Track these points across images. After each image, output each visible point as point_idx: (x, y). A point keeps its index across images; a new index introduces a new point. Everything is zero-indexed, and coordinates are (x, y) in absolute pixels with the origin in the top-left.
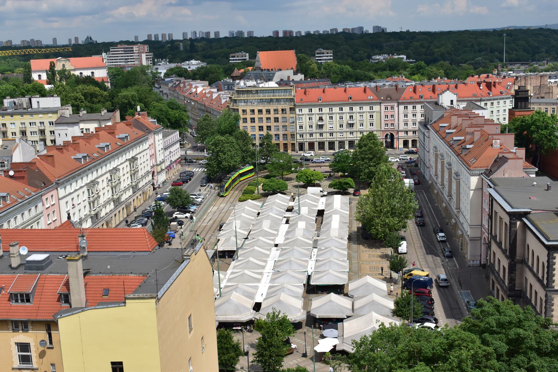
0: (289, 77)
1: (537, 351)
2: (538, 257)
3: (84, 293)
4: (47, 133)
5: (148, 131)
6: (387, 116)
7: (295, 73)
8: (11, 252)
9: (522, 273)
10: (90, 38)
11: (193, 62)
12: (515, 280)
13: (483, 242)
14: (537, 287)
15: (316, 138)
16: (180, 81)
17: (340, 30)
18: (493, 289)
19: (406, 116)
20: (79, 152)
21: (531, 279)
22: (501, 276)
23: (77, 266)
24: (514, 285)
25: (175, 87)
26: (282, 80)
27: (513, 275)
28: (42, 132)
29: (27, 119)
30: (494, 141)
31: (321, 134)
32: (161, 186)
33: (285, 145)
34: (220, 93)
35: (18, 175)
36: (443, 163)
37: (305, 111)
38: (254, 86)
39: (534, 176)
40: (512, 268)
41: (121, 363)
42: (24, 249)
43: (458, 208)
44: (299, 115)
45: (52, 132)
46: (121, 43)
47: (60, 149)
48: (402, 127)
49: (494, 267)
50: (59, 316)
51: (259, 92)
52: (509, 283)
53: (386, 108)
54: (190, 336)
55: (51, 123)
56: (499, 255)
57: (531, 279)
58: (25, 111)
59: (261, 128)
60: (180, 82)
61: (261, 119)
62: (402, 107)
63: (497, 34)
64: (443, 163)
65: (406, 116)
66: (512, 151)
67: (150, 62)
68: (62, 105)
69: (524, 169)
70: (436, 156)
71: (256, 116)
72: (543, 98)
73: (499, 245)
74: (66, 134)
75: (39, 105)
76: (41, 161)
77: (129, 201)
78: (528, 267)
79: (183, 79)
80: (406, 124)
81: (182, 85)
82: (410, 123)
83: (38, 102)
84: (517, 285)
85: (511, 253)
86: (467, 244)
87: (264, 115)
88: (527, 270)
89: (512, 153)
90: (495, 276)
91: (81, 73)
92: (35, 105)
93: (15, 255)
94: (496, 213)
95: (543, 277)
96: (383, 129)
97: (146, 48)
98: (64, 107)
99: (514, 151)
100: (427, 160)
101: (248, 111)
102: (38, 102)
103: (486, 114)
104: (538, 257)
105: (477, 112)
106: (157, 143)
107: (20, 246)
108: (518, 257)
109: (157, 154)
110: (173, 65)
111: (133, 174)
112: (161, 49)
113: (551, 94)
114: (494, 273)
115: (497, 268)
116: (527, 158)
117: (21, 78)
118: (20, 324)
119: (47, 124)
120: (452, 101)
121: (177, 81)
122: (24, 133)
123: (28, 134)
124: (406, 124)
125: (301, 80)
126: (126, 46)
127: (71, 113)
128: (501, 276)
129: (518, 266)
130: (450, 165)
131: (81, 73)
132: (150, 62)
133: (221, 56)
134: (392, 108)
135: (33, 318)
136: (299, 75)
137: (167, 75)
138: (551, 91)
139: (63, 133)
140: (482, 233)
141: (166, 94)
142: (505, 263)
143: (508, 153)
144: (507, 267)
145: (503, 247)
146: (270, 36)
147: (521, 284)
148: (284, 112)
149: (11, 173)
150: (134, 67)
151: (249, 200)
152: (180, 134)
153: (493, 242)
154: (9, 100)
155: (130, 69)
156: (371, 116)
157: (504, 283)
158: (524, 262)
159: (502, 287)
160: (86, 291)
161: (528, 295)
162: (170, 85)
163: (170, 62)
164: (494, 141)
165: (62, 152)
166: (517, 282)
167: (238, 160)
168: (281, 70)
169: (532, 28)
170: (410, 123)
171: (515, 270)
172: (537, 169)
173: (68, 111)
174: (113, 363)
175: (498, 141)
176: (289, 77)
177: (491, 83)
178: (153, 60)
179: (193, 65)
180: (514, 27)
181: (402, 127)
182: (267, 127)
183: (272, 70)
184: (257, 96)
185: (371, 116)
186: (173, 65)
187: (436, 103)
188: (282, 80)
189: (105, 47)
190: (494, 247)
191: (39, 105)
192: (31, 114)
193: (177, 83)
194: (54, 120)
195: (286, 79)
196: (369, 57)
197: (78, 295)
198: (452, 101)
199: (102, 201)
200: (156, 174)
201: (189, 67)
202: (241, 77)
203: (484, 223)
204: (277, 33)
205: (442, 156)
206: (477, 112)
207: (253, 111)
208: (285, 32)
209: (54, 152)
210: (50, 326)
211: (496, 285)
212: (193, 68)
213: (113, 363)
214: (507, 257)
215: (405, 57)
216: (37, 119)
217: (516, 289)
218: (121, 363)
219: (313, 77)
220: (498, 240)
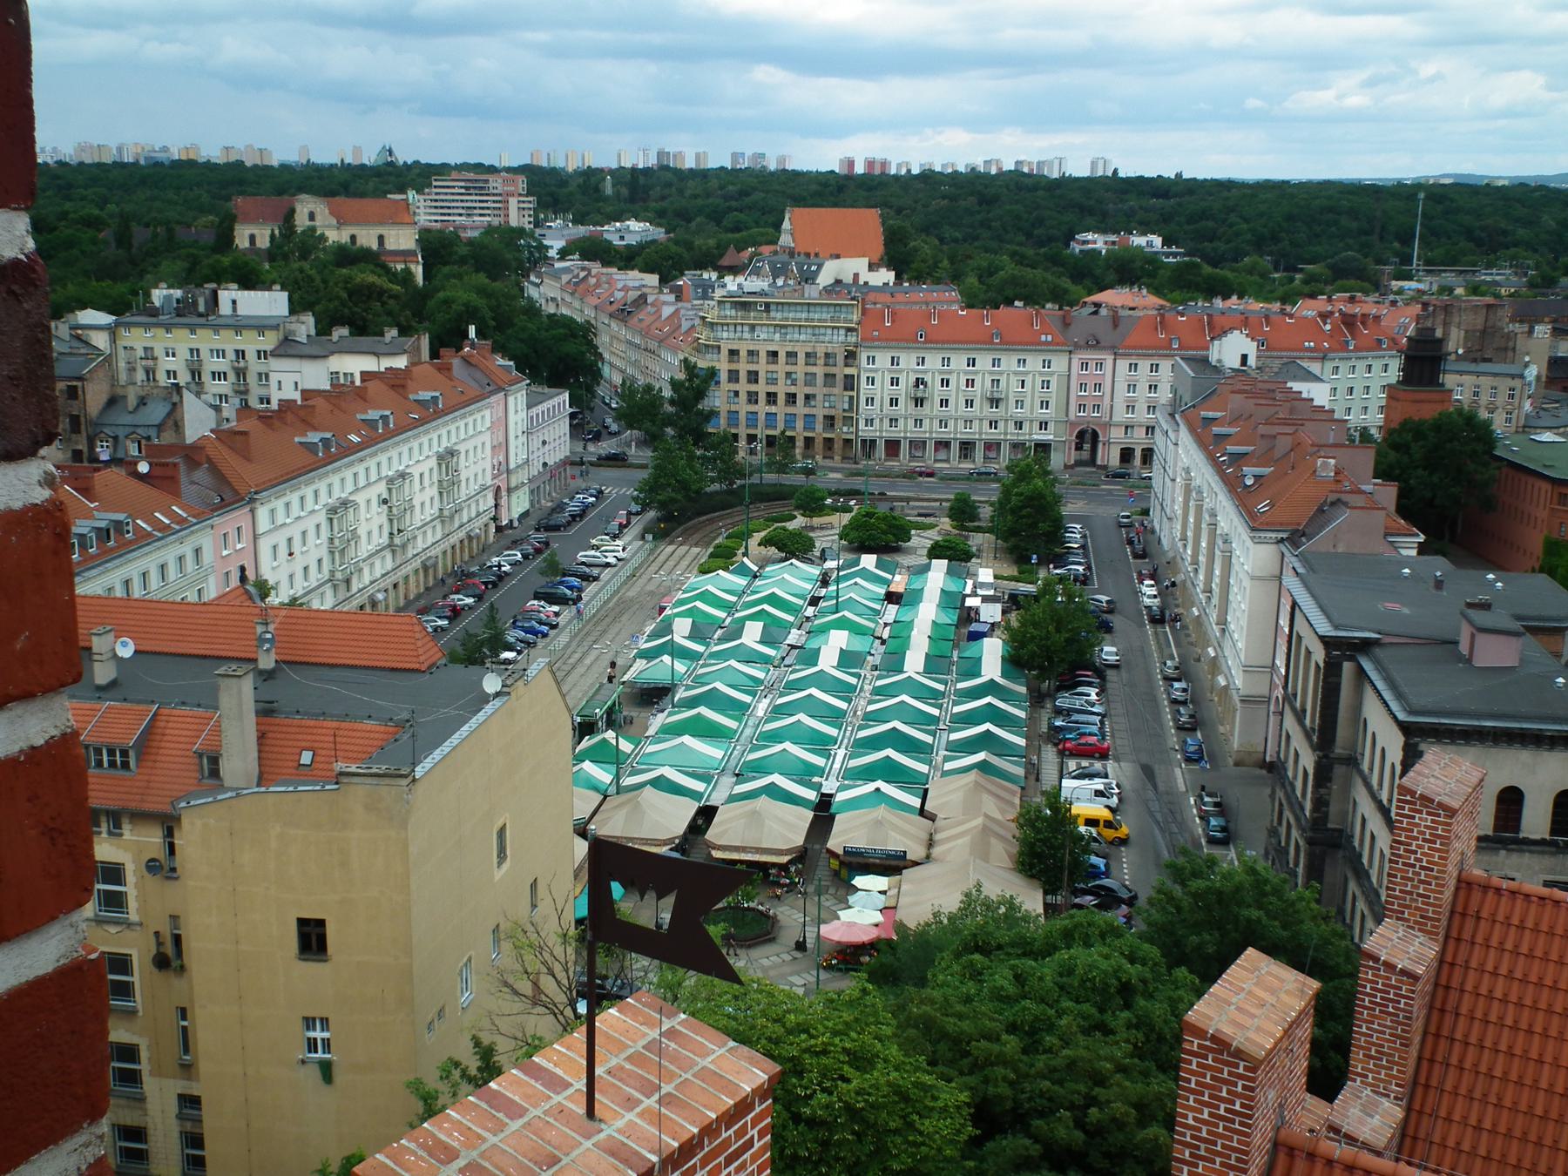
0: (856, 276)
1: (599, 1004)
2: (1383, 750)
3: (256, 755)
4: (252, 379)
5: (498, 387)
6: (1083, 386)
7: (872, 267)
8: (95, 650)
9: (1347, 788)
10: (390, 152)
11: (634, 225)
12: (1327, 804)
13: (1272, 708)
14: (1376, 824)
15: (905, 430)
16: (589, 271)
17: (1008, 165)
18: (1280, 823)
19: (1132, 387)
20: (315, 429)
21: (1366, 807)
22: (1299, 793)
23: (240, 692)
24: (1326, 816)
25: (576, 284)
26: (838, 282)
27: (1322, 791)
28: (241, 373)
29: (205, 340)
30: (1320, 461)
31: (918, 422)
32: (516, 524)
33: (809, 442)
34: (680, 305)
35: (158, 472)
36: (1199, 508)
37: (883, 359)
38: (762, 294)
39: (1414, 553)
40: (1323, 774)
41: (321, 923)
42: (124, 645)
43: (1223, 622)
44: (866, 370)
45: (264, 377)
46: (465, 167)
47: (266, 418)
48: (1121, 415)
49: (1285, 770)
50: (183, 804)
51: (773, 307)
52: (1314, 810)
53: (1084, 365)
54: (498, 874)
55: (260, 354)
56: (1299, 742)
57: (1366, 807)
58: (202, 321)
59: (771, 398)
60: (589, 274)
61: (753, 377)
62: (1123, 365)
63: (1403, 193)
64: (1199, 508)
65: (1132, 387)
66: (1364, 487)
67: (527, 219)
68: (292, 311)
69: (1386, 535)
70: (1188, 490)
71: (762, 366)
72: (1489, 360)
73: (1300, 716)
74: (291, 380)
75: (234, 309)
76: (217, 444)
77: (433, 553)
78: (1361, 772)
79: (596, 267)
80: (1131, 408)
81: (593, 281)
82: (1141, 407)
83: (234, 302)
84: (1332, 817)
85: (1324, 737)
86: (1235, 710)
87: (781, 367)
88: (1359, 782)
89: (1364, 492)
90: (1286, 793)
91: (353, 238)
92: (225, 308)
93: (104, 658)
94: (1299, 638)
95: (1390, 801)
96: (1072, 417)
97: (521, 183)
98: (294, 318)
99: (1368, 488)
100: (1168, 502)
101: (743, 354)
102: (234, 302)
103: (1319, 394)
104: (1383, 750)
105: (1296, 386)
106: (512, 418)
107: (117, 637)
108: (1339, 750)
109: (496, 444)
110: (582, 230)
111: (447, 487)
112: (553, 190)
113: (1510, 354)
114: (1283, 786)
115: (1290, 774)
116: (1404, 510)
117: (208, 238)
118: (103, 819)
119: (251, 356)
120: (1244, 358)
121: (583, 269)
122: (196, 373)
123: (206, 377)
124: (1131, 408)
125: (886, 284)
126: (471, 176)
127: (313, 332)
128: (1299, 793)
129: (1339, 770)
130: (1213, 515)
131: (353, 238)
132: (527, 219)
133: (714, 217)
134: (1100, 365)
135: (133, 805)
136: (883, 271)
137: (564, 254)
138: (1511, 344)
139: (288, 380)
140: (1272, 685)
141: (553, 299)
142: (1308, 760)
143: (1352, 492)
144: (1311, 771)
145: (1308, 722)
146: (832, 172)
147: (1344, 815)
148: (831, 361)
149: (143, 468)
150: (490, 230)
151: (720, 572)
152: (1365, 434)
153: (1287, 707)
154: (165, 292)
155: (476, 234)
156: (1046, 384)
157: (1302, 808)
158: (1352, 761)
159: (1297, 819)
160: (260, 751)
161: (1356, 844)
162: (565, 278)
163: (575, 222)
164: (1320, 461)
165: (270, 426)
166: (1333, 809)
167: (701, 475)
168: (838, 257)
169: (1500, 183)
170: (1141, 407)
171: (1330, 780)
172: (1422, 538)
173: (305, 326)
174: (302, 922)
175: (1332, 461)
176: (856, 276)
177: (1354, 316)
178: (536, 217)
179: (636, 230)
180: (1456, 176)
181: (1121, 415)
182: (769, 394)
183: (816, 255)
184: (768, 318)
185: (1046, 384)
186: (582, 230)
187: (1205, 361)
188: (838, 282)
189: (422, 176)
190: (1290, 723)
191: (234, 309)
192: (216, 328)
193: (582, 274)
194: (269, 347)
195: (848, 279)
196: (1070, 237)
197: (239, 761)
198: (1244, 358)
199: (365, 548)
200: (504, 493)
201: (622, 238)
202: (735, 270)
203: (1278, 662)
204: (851, 164)
205: (1200, 492)
206: (1296, 386)
207: (791, 355)
208: (870, 164)
209: (251, 425)
210: (169, 824)
211: (1287, 814)
212: (631, 240)
213: (302, 922)
214: (1314, 748)
215: (1157, 241)
216: (230, 342)
217: (1330, 826)
218: (321, 923)
219: (918, 278)
220: (1298, 705)
